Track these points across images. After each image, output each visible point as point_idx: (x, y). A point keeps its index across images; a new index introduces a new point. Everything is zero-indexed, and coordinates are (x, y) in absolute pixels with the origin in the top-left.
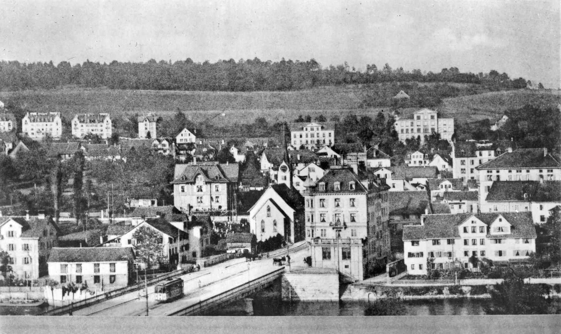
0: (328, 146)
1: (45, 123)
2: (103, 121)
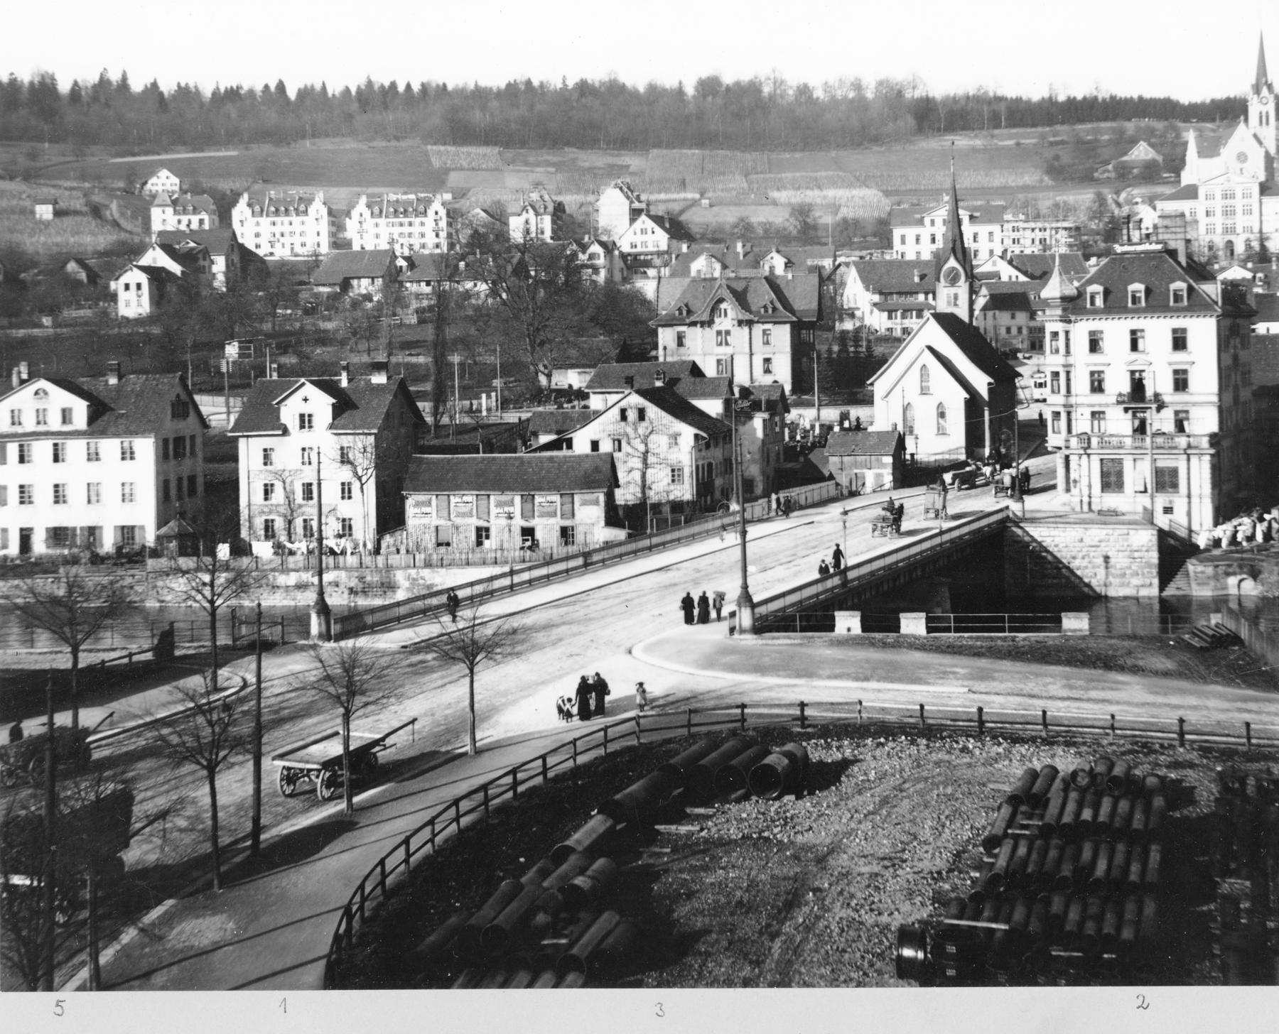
0: (1002, 258)
1: (286, 220)
2: (425, 213)
